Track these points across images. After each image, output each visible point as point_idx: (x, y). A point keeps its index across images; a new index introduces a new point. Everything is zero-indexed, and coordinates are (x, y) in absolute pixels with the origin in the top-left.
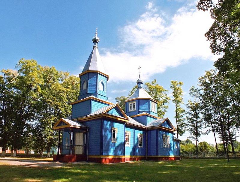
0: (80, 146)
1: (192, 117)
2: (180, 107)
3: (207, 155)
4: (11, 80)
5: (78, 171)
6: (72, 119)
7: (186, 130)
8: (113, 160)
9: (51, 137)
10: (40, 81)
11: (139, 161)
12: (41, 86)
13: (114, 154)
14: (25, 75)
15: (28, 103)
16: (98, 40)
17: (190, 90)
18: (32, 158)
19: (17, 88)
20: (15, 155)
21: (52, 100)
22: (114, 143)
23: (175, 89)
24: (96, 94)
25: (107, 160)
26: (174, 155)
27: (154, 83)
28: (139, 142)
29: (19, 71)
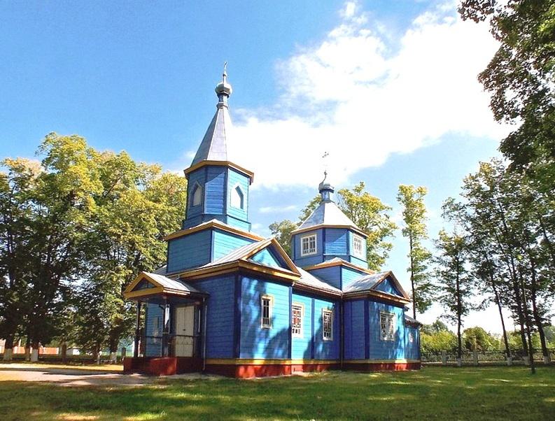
0: (187, 336)
1: (449, 268)
3: (483, 359)
4: (27, 184)
6: (169, 274)
9: (119, 316)
10: (93, 186)
11: (325, 373)
12: (96, 198)
13: (265, 355)
15: (66, 236)
17: (444, 207)
23: (409, 203)
24: (224, 217)
25: (251, 370)
26: (407, 357)
27: (358, 190)
28: (325, 328)
29: (43, 161)
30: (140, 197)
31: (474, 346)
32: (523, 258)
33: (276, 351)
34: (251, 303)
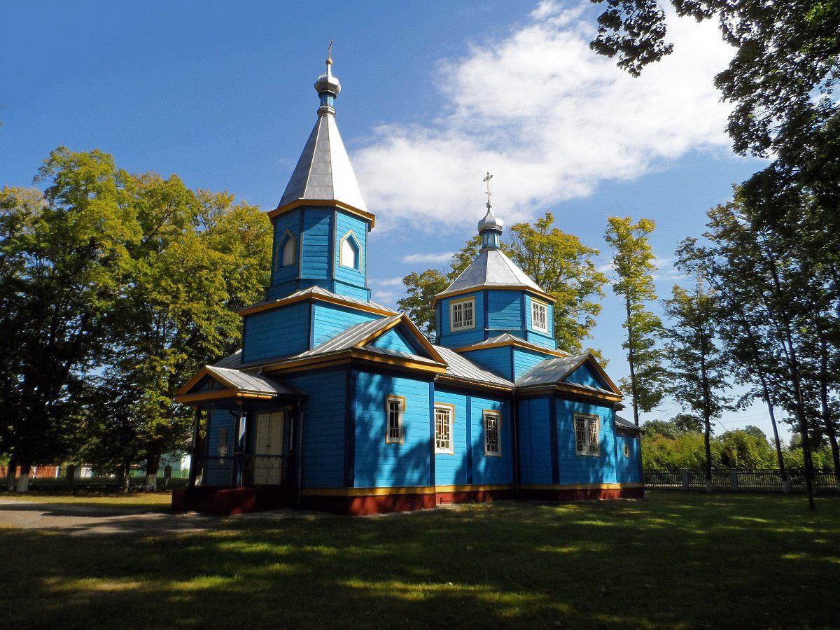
0: (273, 456)
1: (688, 345)
2: (641, 310)
3: (751, 481)
4: (19, 226)
5: (262, 547)
6: (245, 366)
7: (666, 391)
8: (384, 505)
9: (164, 422)
10: (126, 230)
11: (488, 505)
12: (129, 246)
13: (391, 481)
14: (71, 206)
15: (81, 305)
16: (334, 87)
17: (680, 252)
18: (86, 496)
19: (40, 253)
20: (23, 486)
21: (170, 297)
22: (397, 447)
23: (622, 243)
24: (329, 283)
25: (370, 504)
26: (621, 480)
27: (542, 225)
28: (489, 435)
29: (47, 192)
30: (198, 246)
31: (735, 460)
32: (809, 332)
33: (408, 475)
34: (372, 407)
